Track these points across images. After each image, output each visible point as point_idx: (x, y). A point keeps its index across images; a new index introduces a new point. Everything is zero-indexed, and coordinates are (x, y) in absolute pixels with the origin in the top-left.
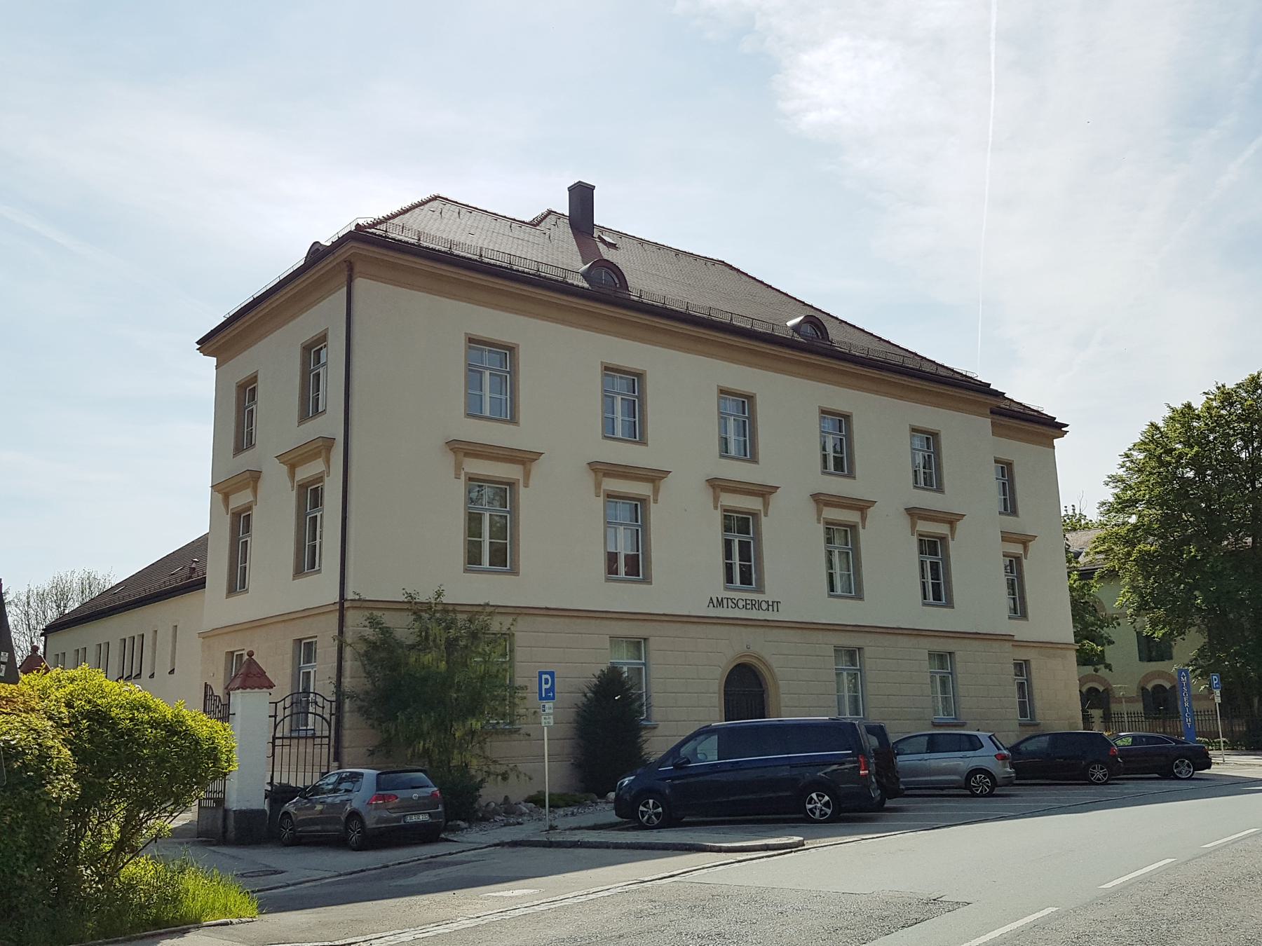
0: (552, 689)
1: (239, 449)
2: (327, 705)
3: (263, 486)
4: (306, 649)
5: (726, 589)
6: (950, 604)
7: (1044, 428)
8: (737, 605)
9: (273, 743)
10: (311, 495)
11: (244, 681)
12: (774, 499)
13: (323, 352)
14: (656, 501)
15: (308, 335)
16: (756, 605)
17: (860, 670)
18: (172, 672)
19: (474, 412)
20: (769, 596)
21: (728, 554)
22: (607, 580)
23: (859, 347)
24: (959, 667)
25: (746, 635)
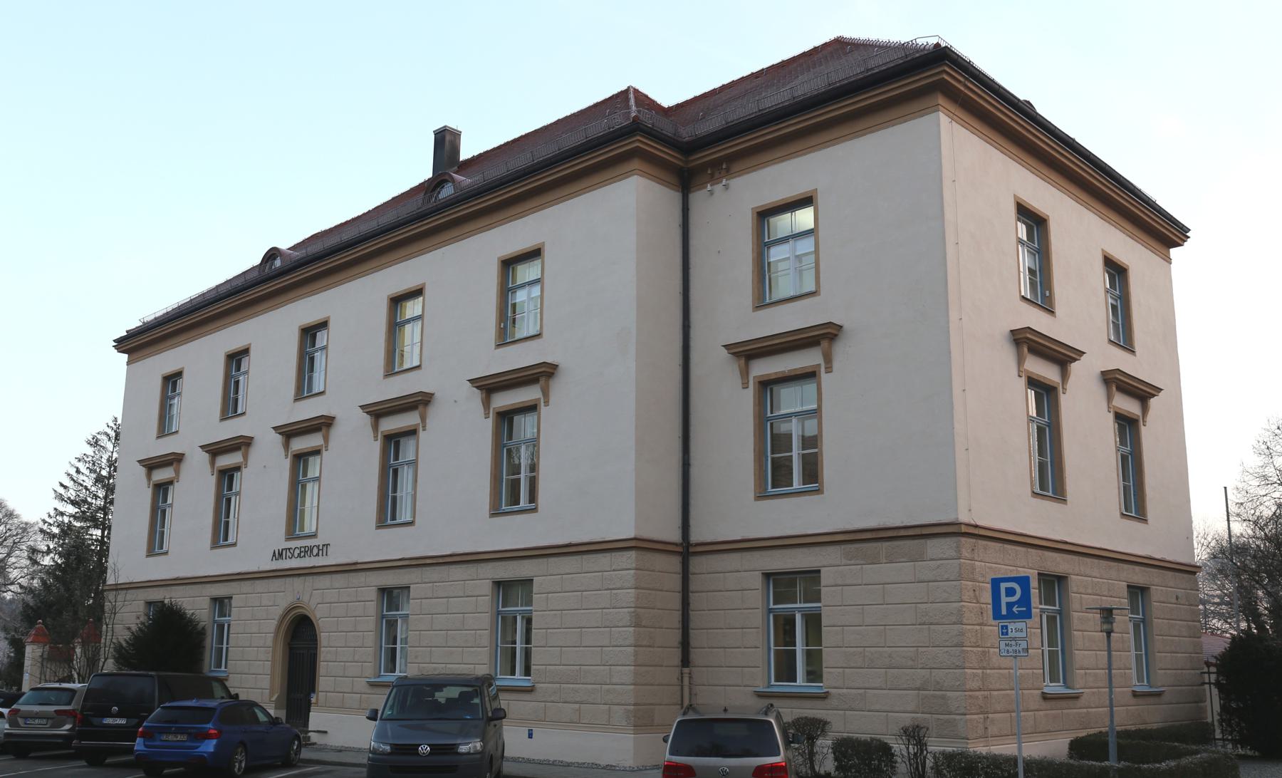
3: (185, 467)
10: (227, 477)
15: (170, 369)
16: (307, 551)
17: (1060, 612)
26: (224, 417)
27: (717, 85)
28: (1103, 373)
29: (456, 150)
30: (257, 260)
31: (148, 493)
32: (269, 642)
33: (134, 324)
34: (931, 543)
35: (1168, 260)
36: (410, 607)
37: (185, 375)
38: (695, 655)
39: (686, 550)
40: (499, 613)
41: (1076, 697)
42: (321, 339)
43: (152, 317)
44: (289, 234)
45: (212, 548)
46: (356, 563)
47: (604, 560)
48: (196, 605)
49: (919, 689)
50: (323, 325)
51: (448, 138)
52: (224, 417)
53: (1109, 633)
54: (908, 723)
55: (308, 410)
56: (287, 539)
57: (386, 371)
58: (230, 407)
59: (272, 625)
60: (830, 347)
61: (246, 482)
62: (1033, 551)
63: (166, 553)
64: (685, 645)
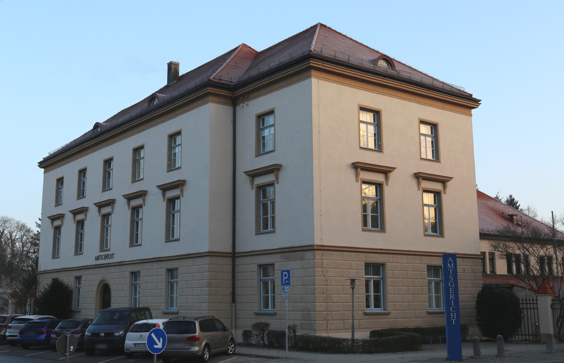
10: (136, 210)
12: (392, 175)
16: (107, 257)
17: (382, 278)
23: (405, 74)
24: (389, 273)
26: (79, 198)
27: (277, 42)
28: (415, 174)
29: (177, 72)
30: (92, 128)
31: (52, 231)
32: (95, 296)
33: (46, 155)
34: (307, 253)
35: (471, 115)
36: (142, 279)
37: (114, 159)
38: (238, 299)
39: (234, 255)
40: (169, 282)
41: (387, 314)
42: (178, 140)
43: (53, 152)
44: (104, 115)
45: (75, 255)
46: (123, 262)
47: (199, 260)
48: (68, 280)
49: (302, 311)
50: (179, 133)
51: (173, 67)
52: (79, 198)
53: (353, 289)
54: (254, 323)
55: (174, 177)
56: (100, 252)
57: (132, 180)
58: (81, 194)
59: (95, 288)
60: (278, 173)
61: (144, 213)
62: (362, 254)
64: (233, 294)
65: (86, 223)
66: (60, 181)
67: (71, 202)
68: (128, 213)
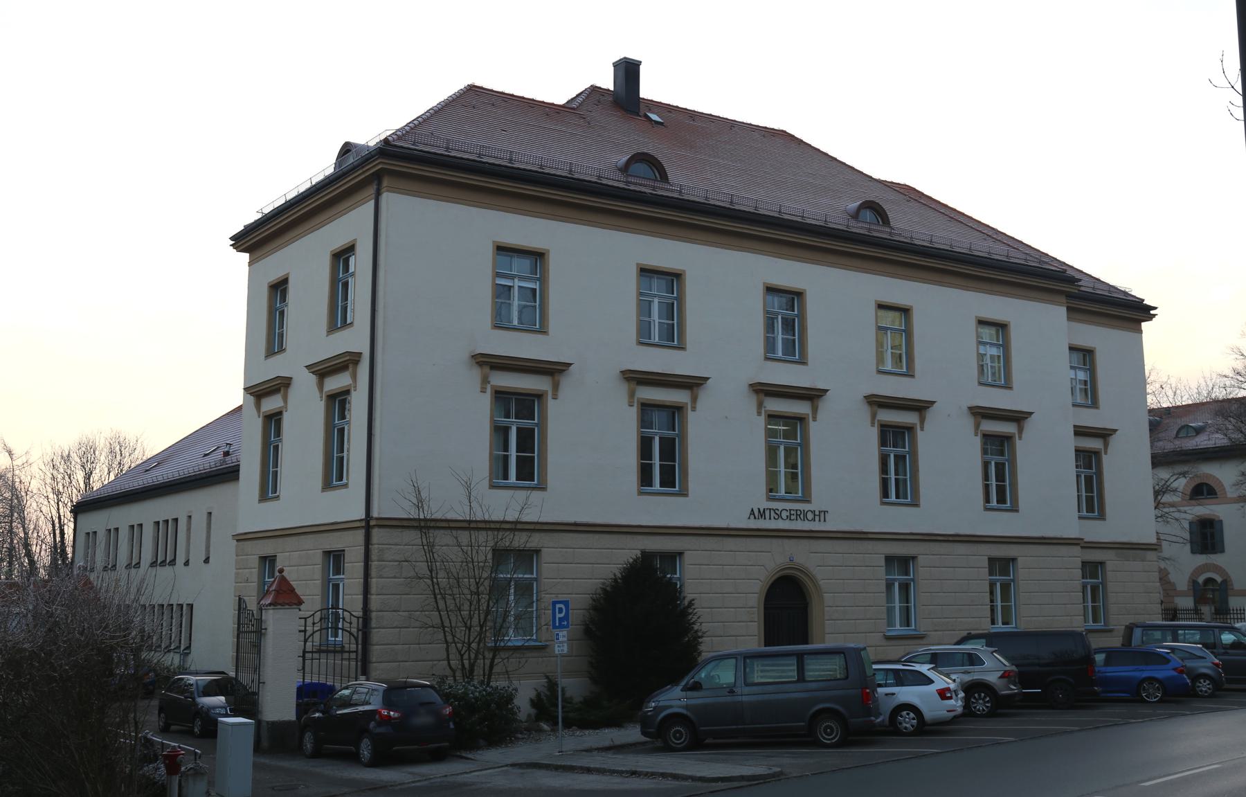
0: (566, 617)
1: (270, 353)
2: (354, 620)
3: (293, 392)
4: (335, 559)
5: (770, 499)
6: (1014, 509)
7: (1130, 312)
8: (780, 516)
9: (304, 657)
10: (338, 402)
11: (276, 597)
13: (352, 260)
14: (694, 409)
15: (339, 243)
18: (207, 561)
19: (500, 323)
20: (815, 505)
21: (986, 477)
22: (641, 493)
25: (790, 546)
33: (240, 228)
35: (1141, 332)
45: (260, 501)
63: (346, 486)
65: (287, 419)
66: (279, 288)
67: (310, 338)
68: (318, 408)
